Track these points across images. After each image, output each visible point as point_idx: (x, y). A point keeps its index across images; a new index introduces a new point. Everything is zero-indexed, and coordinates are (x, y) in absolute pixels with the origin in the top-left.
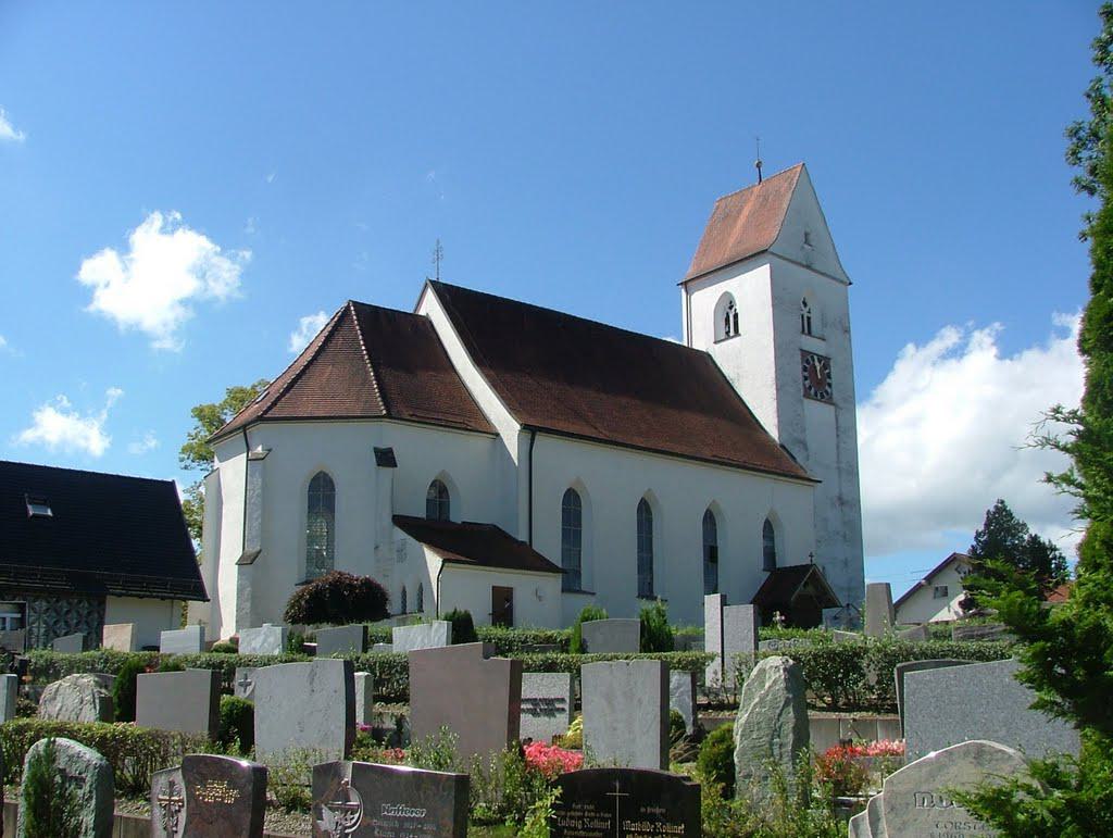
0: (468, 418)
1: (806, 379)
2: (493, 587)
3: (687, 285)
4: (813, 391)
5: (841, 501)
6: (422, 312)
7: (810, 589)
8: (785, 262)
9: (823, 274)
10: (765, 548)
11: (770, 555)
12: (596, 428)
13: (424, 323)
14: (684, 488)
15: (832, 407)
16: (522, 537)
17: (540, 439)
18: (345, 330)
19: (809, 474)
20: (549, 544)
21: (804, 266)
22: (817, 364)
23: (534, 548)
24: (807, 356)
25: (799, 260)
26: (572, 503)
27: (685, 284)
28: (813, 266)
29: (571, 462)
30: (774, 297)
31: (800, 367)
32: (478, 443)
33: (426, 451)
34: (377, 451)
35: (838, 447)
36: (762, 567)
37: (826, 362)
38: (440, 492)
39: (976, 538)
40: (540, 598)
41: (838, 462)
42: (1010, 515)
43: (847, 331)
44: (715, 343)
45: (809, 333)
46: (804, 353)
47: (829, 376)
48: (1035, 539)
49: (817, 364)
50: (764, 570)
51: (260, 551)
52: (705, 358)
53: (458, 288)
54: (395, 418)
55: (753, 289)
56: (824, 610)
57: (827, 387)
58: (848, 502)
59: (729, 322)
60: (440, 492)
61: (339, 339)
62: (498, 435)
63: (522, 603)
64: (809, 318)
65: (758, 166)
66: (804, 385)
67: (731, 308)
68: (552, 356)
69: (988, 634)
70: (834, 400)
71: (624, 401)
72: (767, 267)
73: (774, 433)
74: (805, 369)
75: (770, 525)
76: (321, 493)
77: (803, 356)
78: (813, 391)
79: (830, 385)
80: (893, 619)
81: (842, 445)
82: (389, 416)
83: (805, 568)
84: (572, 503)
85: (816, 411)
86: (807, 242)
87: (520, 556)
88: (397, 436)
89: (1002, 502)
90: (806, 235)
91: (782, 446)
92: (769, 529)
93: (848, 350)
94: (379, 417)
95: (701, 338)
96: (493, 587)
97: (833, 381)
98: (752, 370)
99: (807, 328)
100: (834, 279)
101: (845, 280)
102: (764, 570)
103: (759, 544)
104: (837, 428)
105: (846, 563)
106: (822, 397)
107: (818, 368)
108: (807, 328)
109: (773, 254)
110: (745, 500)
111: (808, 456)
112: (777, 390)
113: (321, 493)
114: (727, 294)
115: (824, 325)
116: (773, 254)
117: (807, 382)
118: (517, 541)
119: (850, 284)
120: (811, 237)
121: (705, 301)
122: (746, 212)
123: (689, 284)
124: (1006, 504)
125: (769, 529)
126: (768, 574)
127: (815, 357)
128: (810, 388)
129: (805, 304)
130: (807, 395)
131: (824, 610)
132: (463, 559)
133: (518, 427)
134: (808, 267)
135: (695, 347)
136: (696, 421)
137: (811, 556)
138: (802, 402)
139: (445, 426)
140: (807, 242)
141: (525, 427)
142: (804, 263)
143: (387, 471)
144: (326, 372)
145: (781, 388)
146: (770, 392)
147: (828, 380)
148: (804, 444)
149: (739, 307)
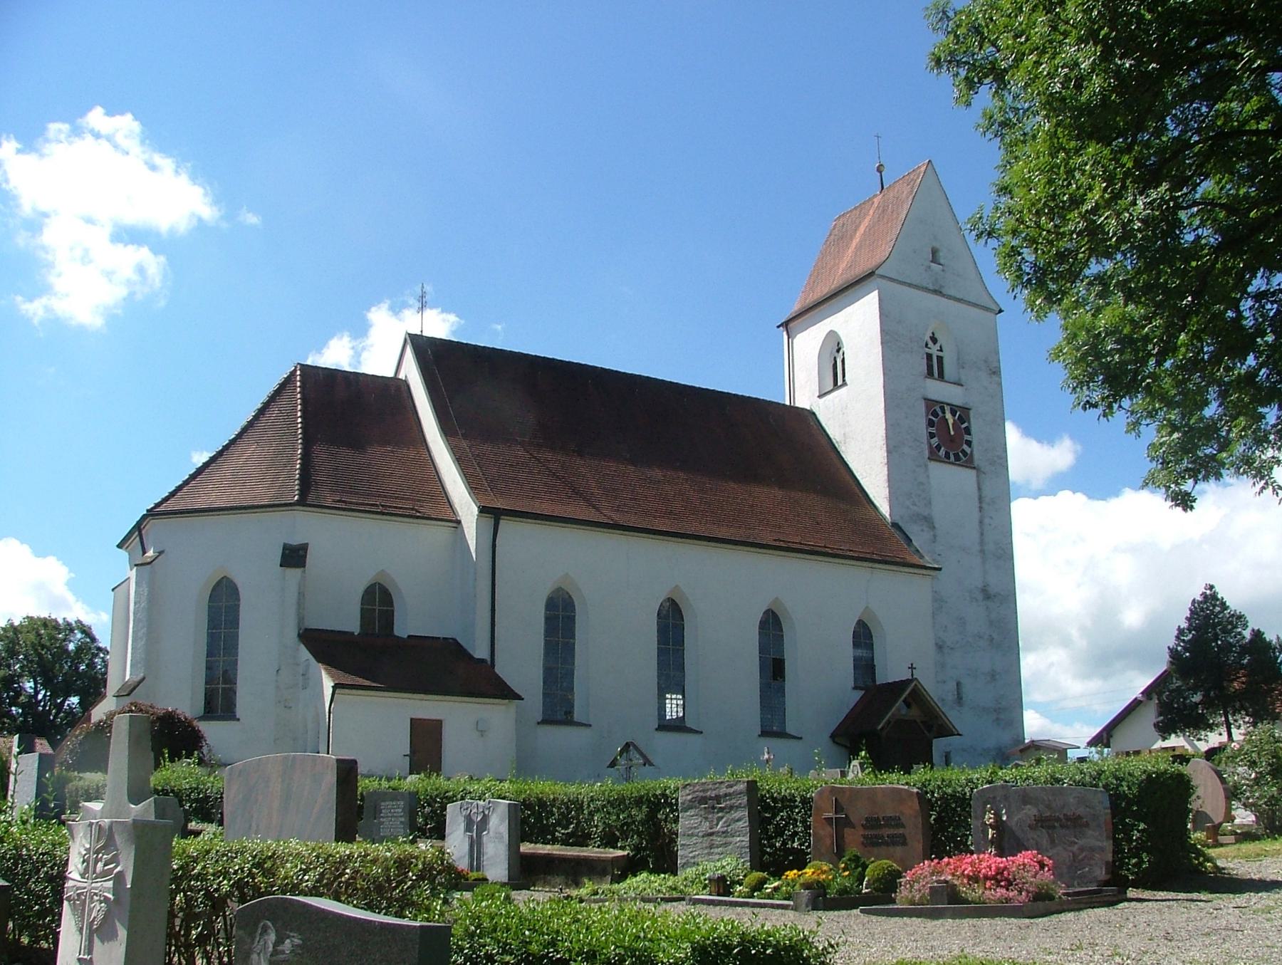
0: (426, 502)
1: (932, 435)
2: (414, 722)
3: (789, 325)
4: (942, 452)
5: (987, 594)
6: (402, 376)
7: (914, 713)
8: (889, 283)
9: (959, 300)
10: (856, 660)
11: (865, 667)
12: (598, 510)
13: (404, 388)
14: (727, 586)
15: (974, 472)
16: (481, 652)
17: (506, 525)
18: (283, 401)
19: (928, 560)
20: (522, 661)
21: (926, 290)
22: (948, 416)
23: (497, 670)
24: (934, 409)
25: (925, 285)
26: (561, 616)
27: (786, 325)
28: (944, 291)
29: (551, 555)
30: (884, 331)
31: (923, 422)
32: (431, 535)
33: (353, 550)
34: (304, 548)
35: (981, 522)
36: (852, 684)
37: (962, 414)
38: (379, 600)
39: (1178, 637)
40: (482, 733)
41: (982, 543)
42: (1224, 606)
43: (996, 372)
44: (819, 397)
45: (941, 376)
46: (930, 403)
47: (968, 431)
48: (1257, 634)
49: (948, 416)
50: (855, 688)
51: (143, 679)
52: (808, 417)
53: (476, 347)
54: (310, 506)
55: (859, 323)
56: (935, 741)
57: (965, 447)
58: (997, 598)
59: (834, 372)
60: (379, 600)
61: (274, 411)
62: (459, 522)
63: (453, 744)
64: (940, 359)
65: (880, 170)
66: (930, 446)
67: (838, 351)
68: (569, 428)
69: (726, 795)
70: (976, 463)
71: (657, 474)
72: (876, 293)
73: (884, 508)
74: (931, 424)
75: (869, 635)
76: (223, 605)
77: (928, 408)
78: (942, 452)
79: (969, 443)
80: (651, 764)
81: (987, 521)
82: (302, 502)
83: (903, 684)
84: (561, 616)
85: (949, 480)
86: (935, 259)
87: (482, 681)
88: (309, 527)
89: (1211, 587)
90: (934, 252)
91: (895, 525)
92: (863, 635)
93: (997, 396)
94: (290, 505)
95: (804, 394)
96: (414, 722)
97: (975, 437)
98: (859, 427)
99: (935, 368)
100: (975, 305)
101: (994, 307)
102: (855, 688)
103: (846, 655)
104: (980, 499)
105: (993, 676)
106: (957, 458)
107: (951, 422)
108: (935, 368)
109: (882, 277)
110: (823, 598)
111: (935, 536)
112: (889, 452)
113: (223, 605)
114: (832, 334)
115: (961, 365)
116: (882, 277)
117: (935, 441)
118: (471, 657)
119: (1001, 311)
120: (942, 255)
121: (809, 342)
122: (862, 229)
123: (791, 325)
124: (1217, 589)
125: (863, 635)
126: (860, 693)
127: (947, 409)
128: (938, 448)
129: (934, 340)
130: (933, 456)
131: (935, 741)
132: (367, 683)
133: (475, 510)
134: (937, 292)
135: (799, 404)
136: (767, 496)
137: (912, 668)
138: (926, 466)
139: (383, 514)
140: (935, 259)
141: (483, 510)
142: (931, 287)
143: (294, 574)
144: (250, 449)
145: (893, 449)
146: (880, 455)
147: (967, 437)
148: (928, 521)
149: (845, 349)
